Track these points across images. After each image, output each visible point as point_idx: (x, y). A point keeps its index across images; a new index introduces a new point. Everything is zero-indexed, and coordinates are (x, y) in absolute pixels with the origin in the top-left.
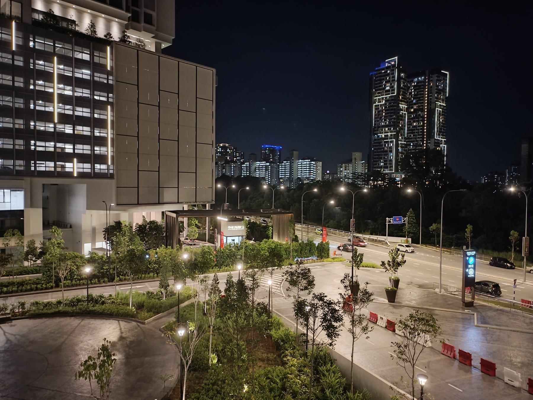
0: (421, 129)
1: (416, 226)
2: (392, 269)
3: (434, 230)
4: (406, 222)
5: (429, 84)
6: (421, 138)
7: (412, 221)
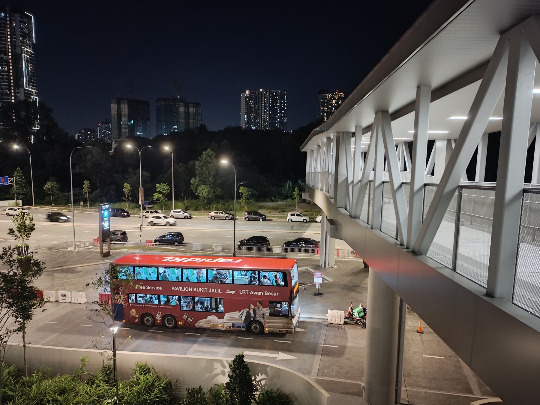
0: (6, 75)
1: (26, 186)
2: (24, 236)
3: (49, 189)
4: (14, 183)
5: (11, 24)
6: (7, 85)
7: (21, 181)
